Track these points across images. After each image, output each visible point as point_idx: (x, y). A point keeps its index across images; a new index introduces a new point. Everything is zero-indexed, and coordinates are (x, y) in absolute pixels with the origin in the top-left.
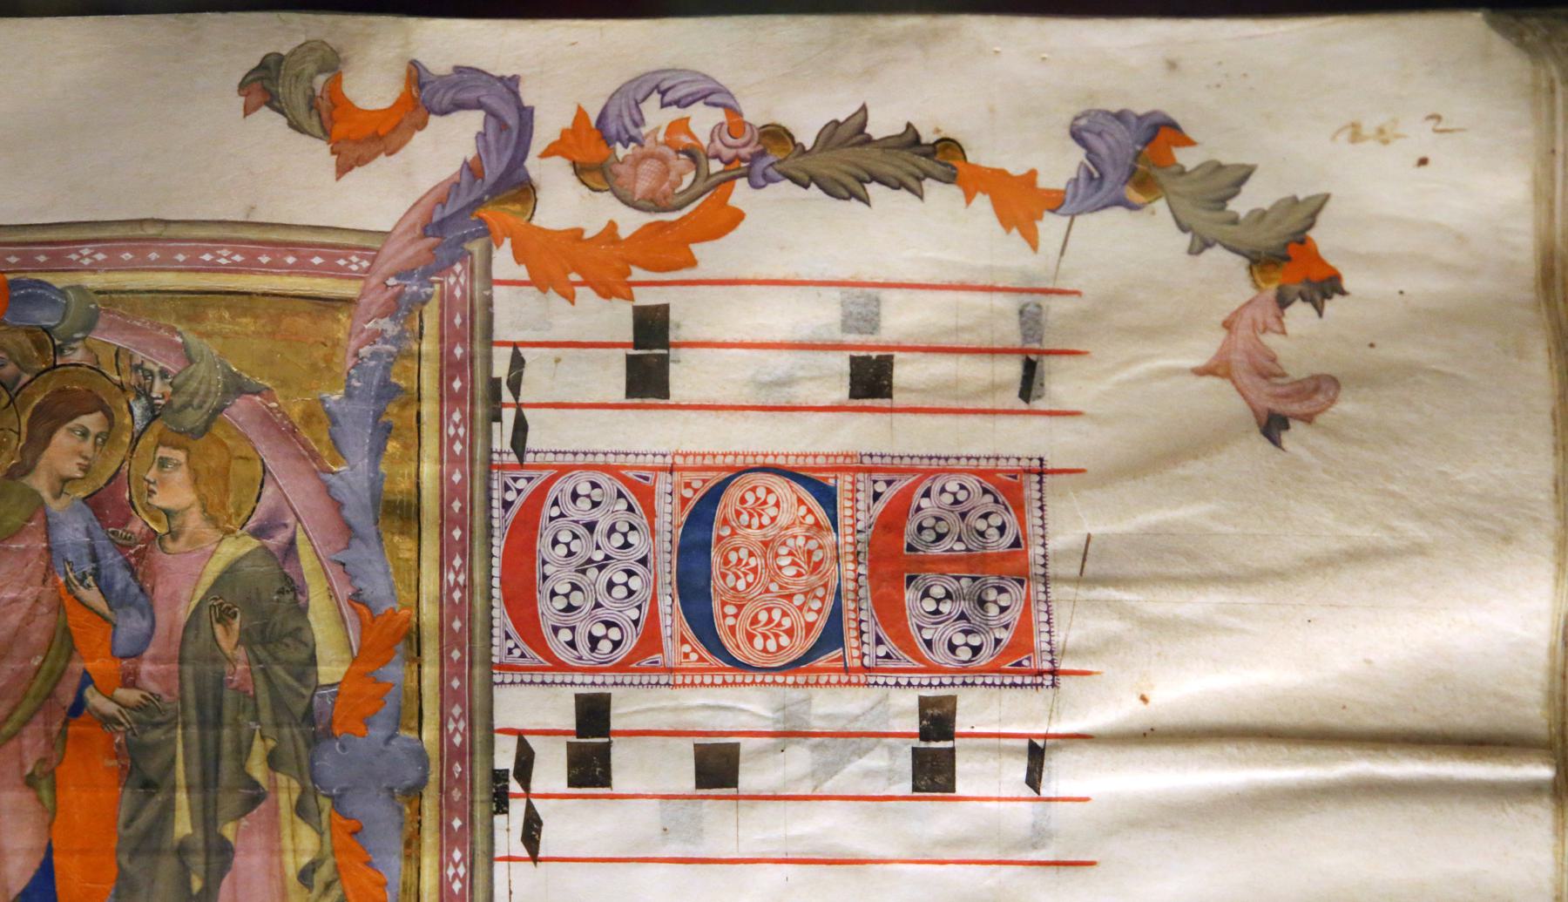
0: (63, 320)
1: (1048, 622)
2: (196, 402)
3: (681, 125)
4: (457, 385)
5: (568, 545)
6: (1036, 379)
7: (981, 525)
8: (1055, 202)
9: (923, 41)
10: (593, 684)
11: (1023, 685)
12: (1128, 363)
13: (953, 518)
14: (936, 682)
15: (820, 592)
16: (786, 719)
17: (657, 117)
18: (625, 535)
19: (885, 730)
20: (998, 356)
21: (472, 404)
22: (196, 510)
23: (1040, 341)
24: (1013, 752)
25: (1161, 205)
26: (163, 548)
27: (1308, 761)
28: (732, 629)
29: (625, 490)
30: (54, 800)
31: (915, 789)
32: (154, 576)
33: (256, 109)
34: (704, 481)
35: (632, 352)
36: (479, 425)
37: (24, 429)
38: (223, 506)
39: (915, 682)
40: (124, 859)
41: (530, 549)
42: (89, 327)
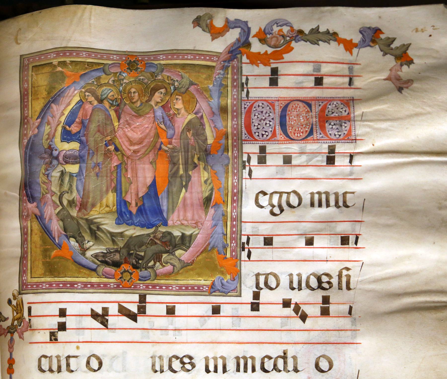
0: (157, 70)
1: (355, 129)
2: (183, 87)
3: (281, 30)
4: (235, 84)
5: (257, 116)
6: (352, 82)
7: (341, 110)
8: (356, 46)
9: (330, 12)
10: (263, 144)
11: (349, 142)
12: (370, 78)
13: (336, 109)
14: (332, 142)
15: (309, 124)
16: (301, 150)
17: (276, 29)
18: (269, 114)
19: (321, 152)
20: (344, 77)
21: (238, 88)
22: (183, 109)
23: (353, 74)
24: (347, 156)
25: (377, 46)
26: (176, 117)
27: (406, 157)
28: (291, 132)
29: (269, 105)
30: (156, 167)
31: (327, 164)
32: (175, 122)
33: (196, 27)
34: (285, 103)
35: (270, 77)
36: (239, 92)
37: (149, 92)
38: (189, 108)
39: (327, 142)
40: (170, 178)
41: (250, 117)
42: (162, 71)
